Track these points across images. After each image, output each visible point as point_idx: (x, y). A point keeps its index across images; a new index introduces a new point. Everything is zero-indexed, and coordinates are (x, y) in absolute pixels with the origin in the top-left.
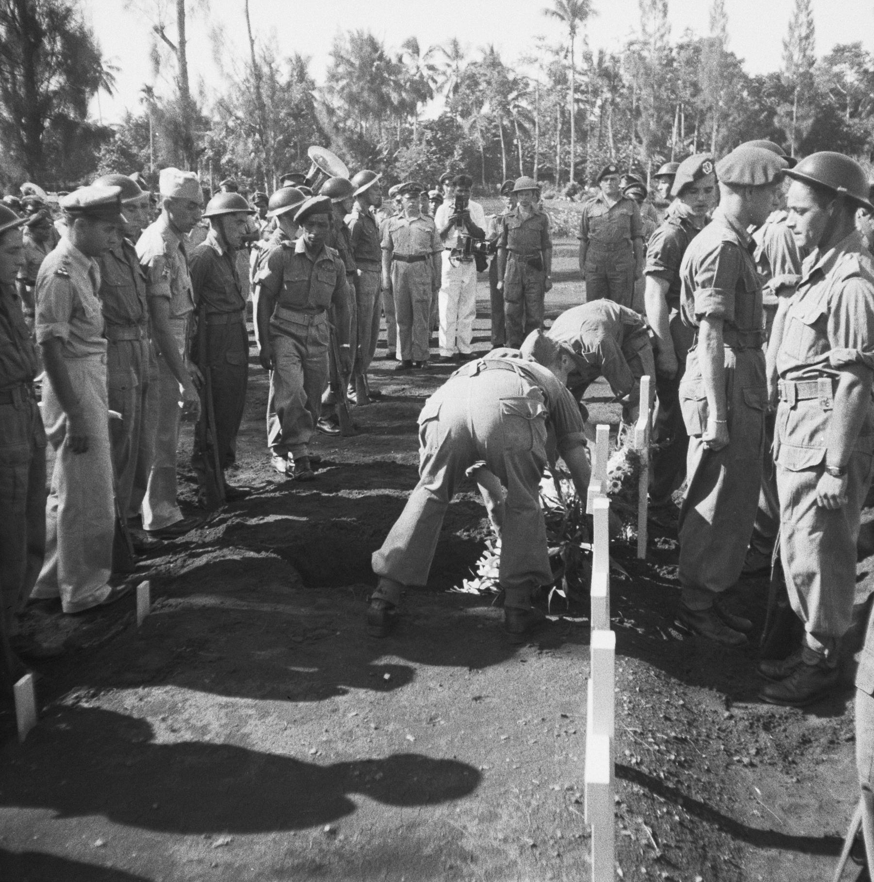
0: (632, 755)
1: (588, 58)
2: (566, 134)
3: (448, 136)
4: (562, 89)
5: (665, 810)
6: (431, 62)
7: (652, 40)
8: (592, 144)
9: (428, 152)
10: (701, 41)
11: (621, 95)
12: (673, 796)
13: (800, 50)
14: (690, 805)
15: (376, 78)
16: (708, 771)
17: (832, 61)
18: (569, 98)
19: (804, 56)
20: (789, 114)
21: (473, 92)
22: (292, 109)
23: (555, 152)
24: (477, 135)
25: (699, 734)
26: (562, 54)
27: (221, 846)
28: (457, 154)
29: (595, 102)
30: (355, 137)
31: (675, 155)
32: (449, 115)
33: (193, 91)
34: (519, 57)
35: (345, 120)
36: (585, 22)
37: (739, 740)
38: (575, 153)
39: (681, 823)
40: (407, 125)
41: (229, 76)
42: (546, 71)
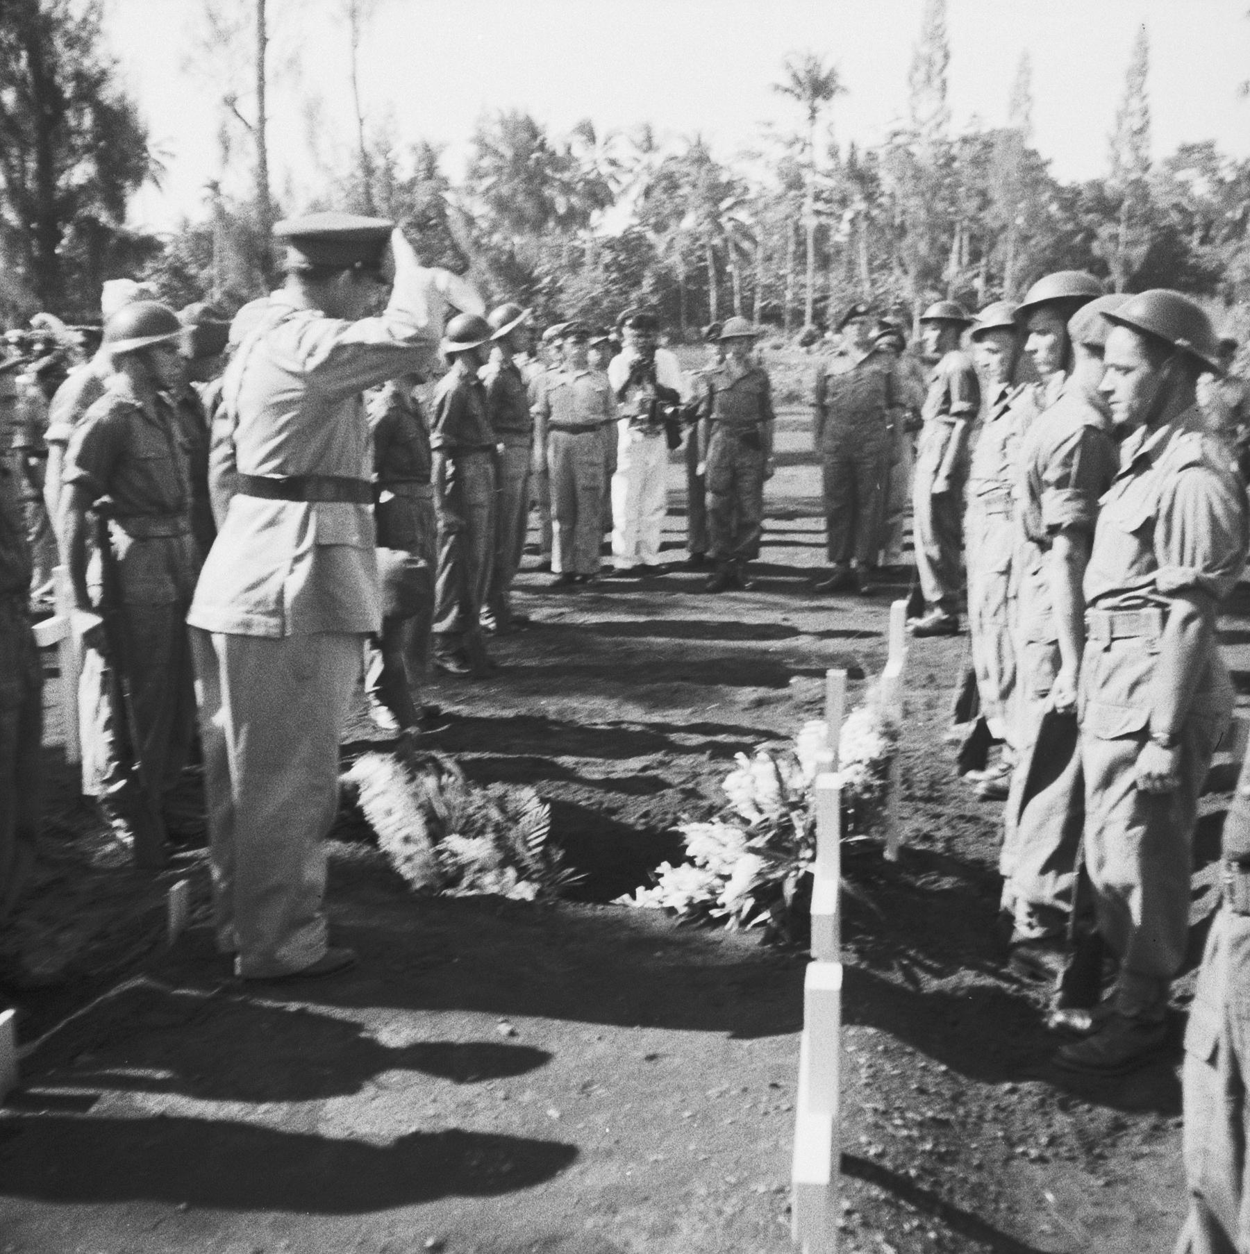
0: (870, 1144)
1: (833, 153)
2: (801, 258)
6: (613, 155)
7: (924, 131)
8: (837, 276)
12: (929, 1204)
14: (952, 1216)
15: (536, 178)
16: (980, 1167)
17: (1175, 165)
18: (809, 205)
20: (1114, 238)
24: (675, 258)
26: (798, 147)
28: (647, 283)
30: (504, 258)
32: (636, 229)
42: (775, 171)
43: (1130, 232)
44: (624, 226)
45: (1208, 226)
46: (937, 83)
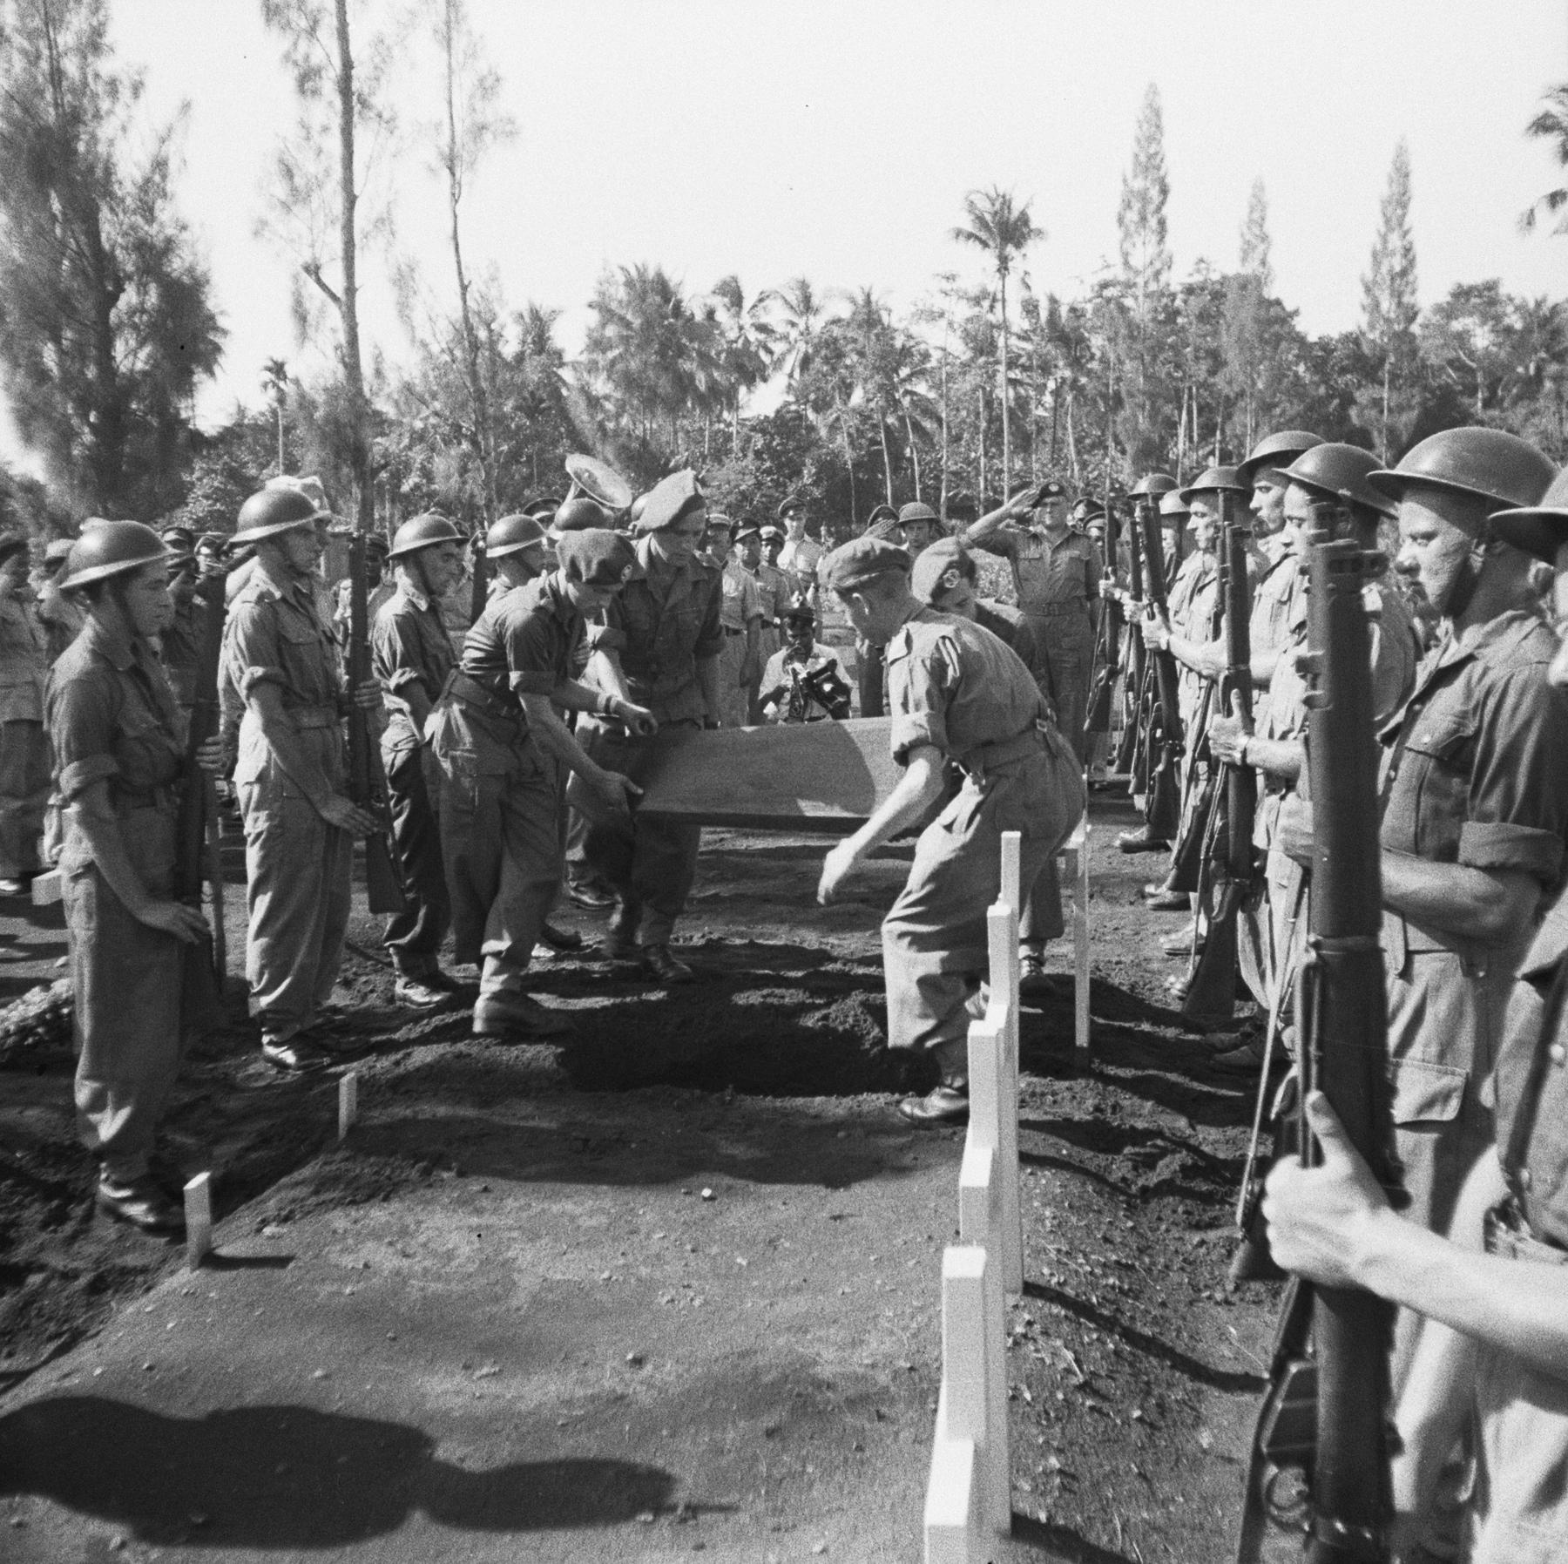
0: (1052, 1275)
1: (1030, 308)
2: (994, 438)
3: (791, 445)
4: (987, 363)
5: (1095, 1336)
6: (764, 320)
7: (1140, 280)
8: (1040, 459)
9: (758, 469)
10: (1224, 280)
11: (1089, 373)
12: (1107, 1325)
13: (1392, 295)
14: (1129, 1335)
15: (669, 345)
16: (1163, 1304)
17: (1449, 312)
18: (1000, 378)
19: (1399, 304)
20: (1377, 403)
21: (834, 369)
22: (525, 399)
23: (977, 469)
24: (841, 440)
25: (1154, 1263)
26: (986, 304)
27: (487, 1376)
28: (808, 472)
29: (1045, 385)
30: (635, 445)
31: (1184, 475)
32: (793, 407)
33: (367, 367)
34: (913, 309)
35: (618, 416)
36: (1023, 251)
37: (1211, 1273)
38: (1010, 470)
39: (1117, 1353)
40: (722, 426)
41: (424, 345)
42: (959, 333)
43: (1395, 395)
44: (777, 404)
45: (1492, 388)
46: (1153, 222)
